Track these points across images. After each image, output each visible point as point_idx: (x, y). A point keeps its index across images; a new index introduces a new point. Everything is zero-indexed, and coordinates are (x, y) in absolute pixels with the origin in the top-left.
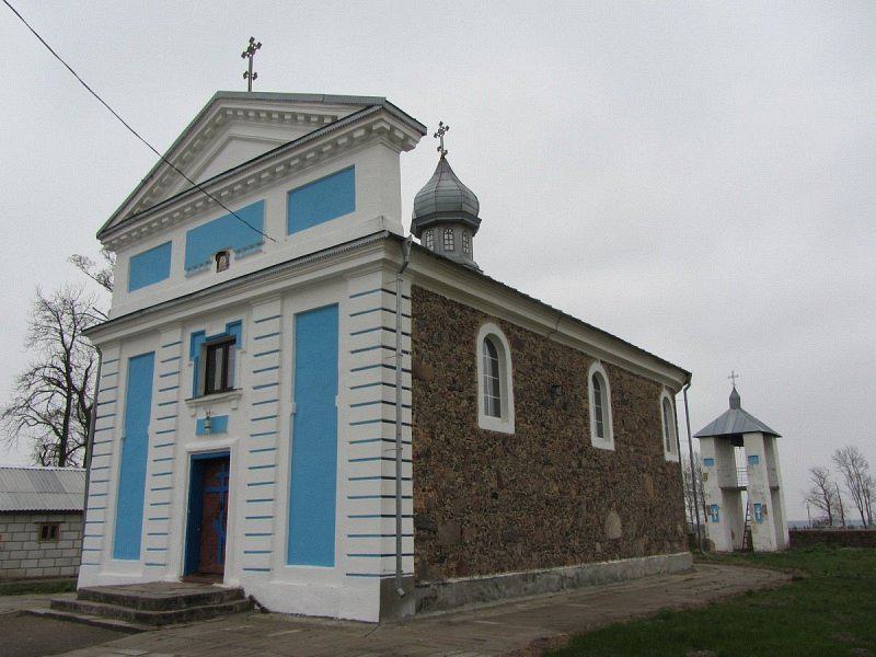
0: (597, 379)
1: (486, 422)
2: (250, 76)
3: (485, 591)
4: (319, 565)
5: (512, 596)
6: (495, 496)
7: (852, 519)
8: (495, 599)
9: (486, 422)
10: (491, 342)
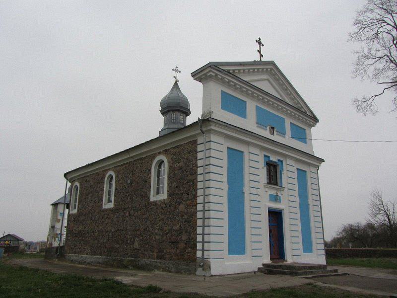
0: (111, 177)
1: (153, 198)
2: (261, 56)
4: (232, 255)
9: (153, 198)
10: (111, 177)
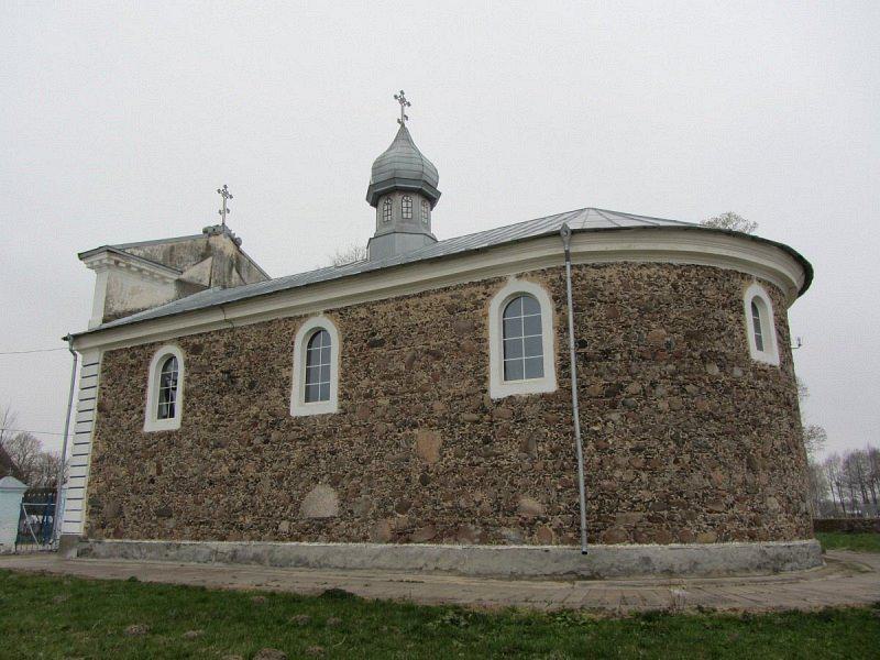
1: (298, 408)
3: (129, 551)
5: (151, 558)
6: (152, 481)
7: (816, 461)
8: (135, 558)
9: (298, 408)
